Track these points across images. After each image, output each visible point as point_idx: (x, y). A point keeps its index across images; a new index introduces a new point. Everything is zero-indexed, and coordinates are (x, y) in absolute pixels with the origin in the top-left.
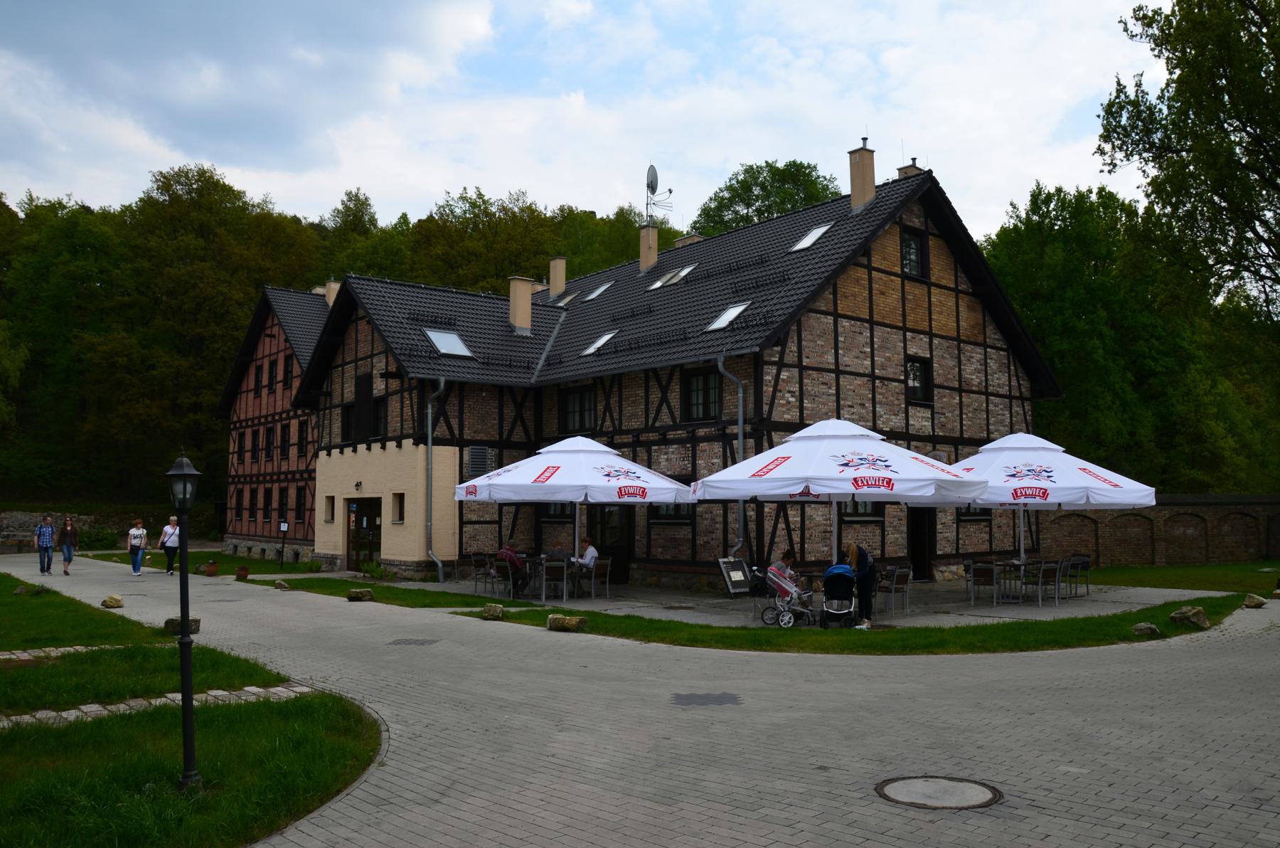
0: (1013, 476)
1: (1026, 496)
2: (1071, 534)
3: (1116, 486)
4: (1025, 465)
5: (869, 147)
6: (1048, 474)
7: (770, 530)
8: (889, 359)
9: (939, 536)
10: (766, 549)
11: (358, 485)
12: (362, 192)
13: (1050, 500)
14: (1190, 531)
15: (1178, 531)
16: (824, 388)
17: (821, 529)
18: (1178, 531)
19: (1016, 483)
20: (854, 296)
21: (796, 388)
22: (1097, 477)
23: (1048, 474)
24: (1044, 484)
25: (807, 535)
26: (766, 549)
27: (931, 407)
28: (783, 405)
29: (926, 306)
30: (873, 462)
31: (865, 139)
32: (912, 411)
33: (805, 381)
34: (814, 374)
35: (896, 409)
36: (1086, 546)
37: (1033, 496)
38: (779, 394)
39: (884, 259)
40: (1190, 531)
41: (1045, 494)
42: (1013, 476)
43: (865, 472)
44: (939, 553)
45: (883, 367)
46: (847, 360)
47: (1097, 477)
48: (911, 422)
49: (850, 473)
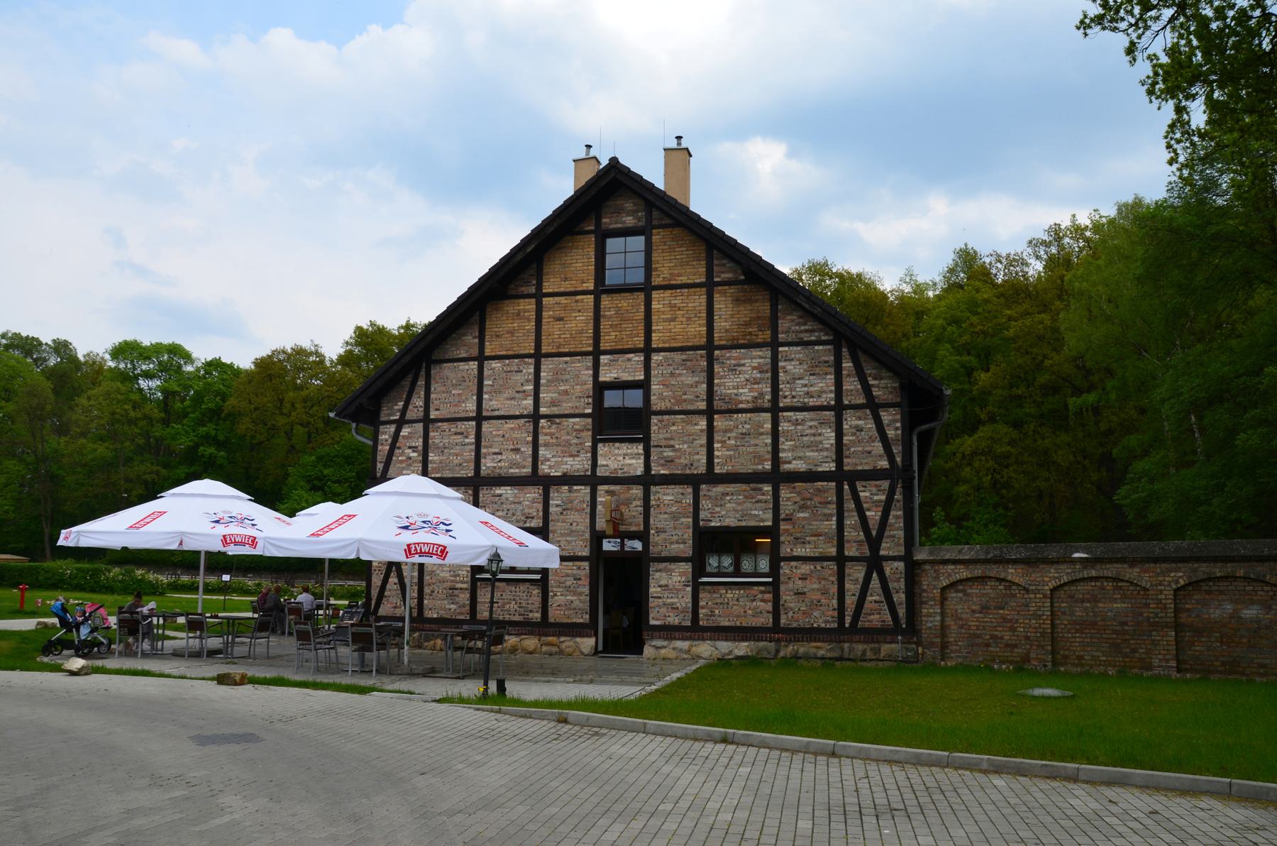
0: (406, 528)
1: (421, 554)
2: (984, 609)
3: (521, 544)
4: (419, 515)
5: (684, 144)
6: (447, 527)
7: (379, 584)
8: (566, 393)
9: (653, 603)
10: (373, 603)
11: (181, 543)
12: (969, 247)
13: (448, 560)
14: (1250, 613)
15: (1220, 610)
16: (459, 439)
17: (448, 584)
18: (1220, 610)
19: (409, 537)
20: (512, 333)
21: (419, 443)
22: (500, 532)
23: (447, 527)
24: (442, 539)
25: (427, 590)
26: (373, 603)
27: (646, 441)
28: (401, 462)
29: (641, 315)
30: (242, 521)
31: (679, 138)
32: (602, 449)
33: (431, 434)
34: (445, 425)
35: (573, 449)
36: (1013, 629)
37: (429, 554)
38: (397, 451)
39: (566, 279)
40: (1250, 613)
41: (443, 552)
42: (406, 528)
43: (234, 529)
44: (652, 622)
45: (553, 403)
46: (492, 404)
47: (500, 532)
48: (601, 461)
49: (221, 530)
